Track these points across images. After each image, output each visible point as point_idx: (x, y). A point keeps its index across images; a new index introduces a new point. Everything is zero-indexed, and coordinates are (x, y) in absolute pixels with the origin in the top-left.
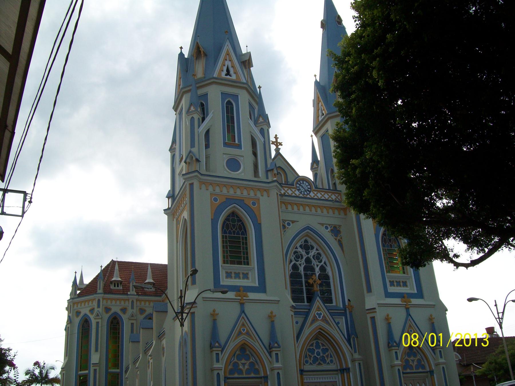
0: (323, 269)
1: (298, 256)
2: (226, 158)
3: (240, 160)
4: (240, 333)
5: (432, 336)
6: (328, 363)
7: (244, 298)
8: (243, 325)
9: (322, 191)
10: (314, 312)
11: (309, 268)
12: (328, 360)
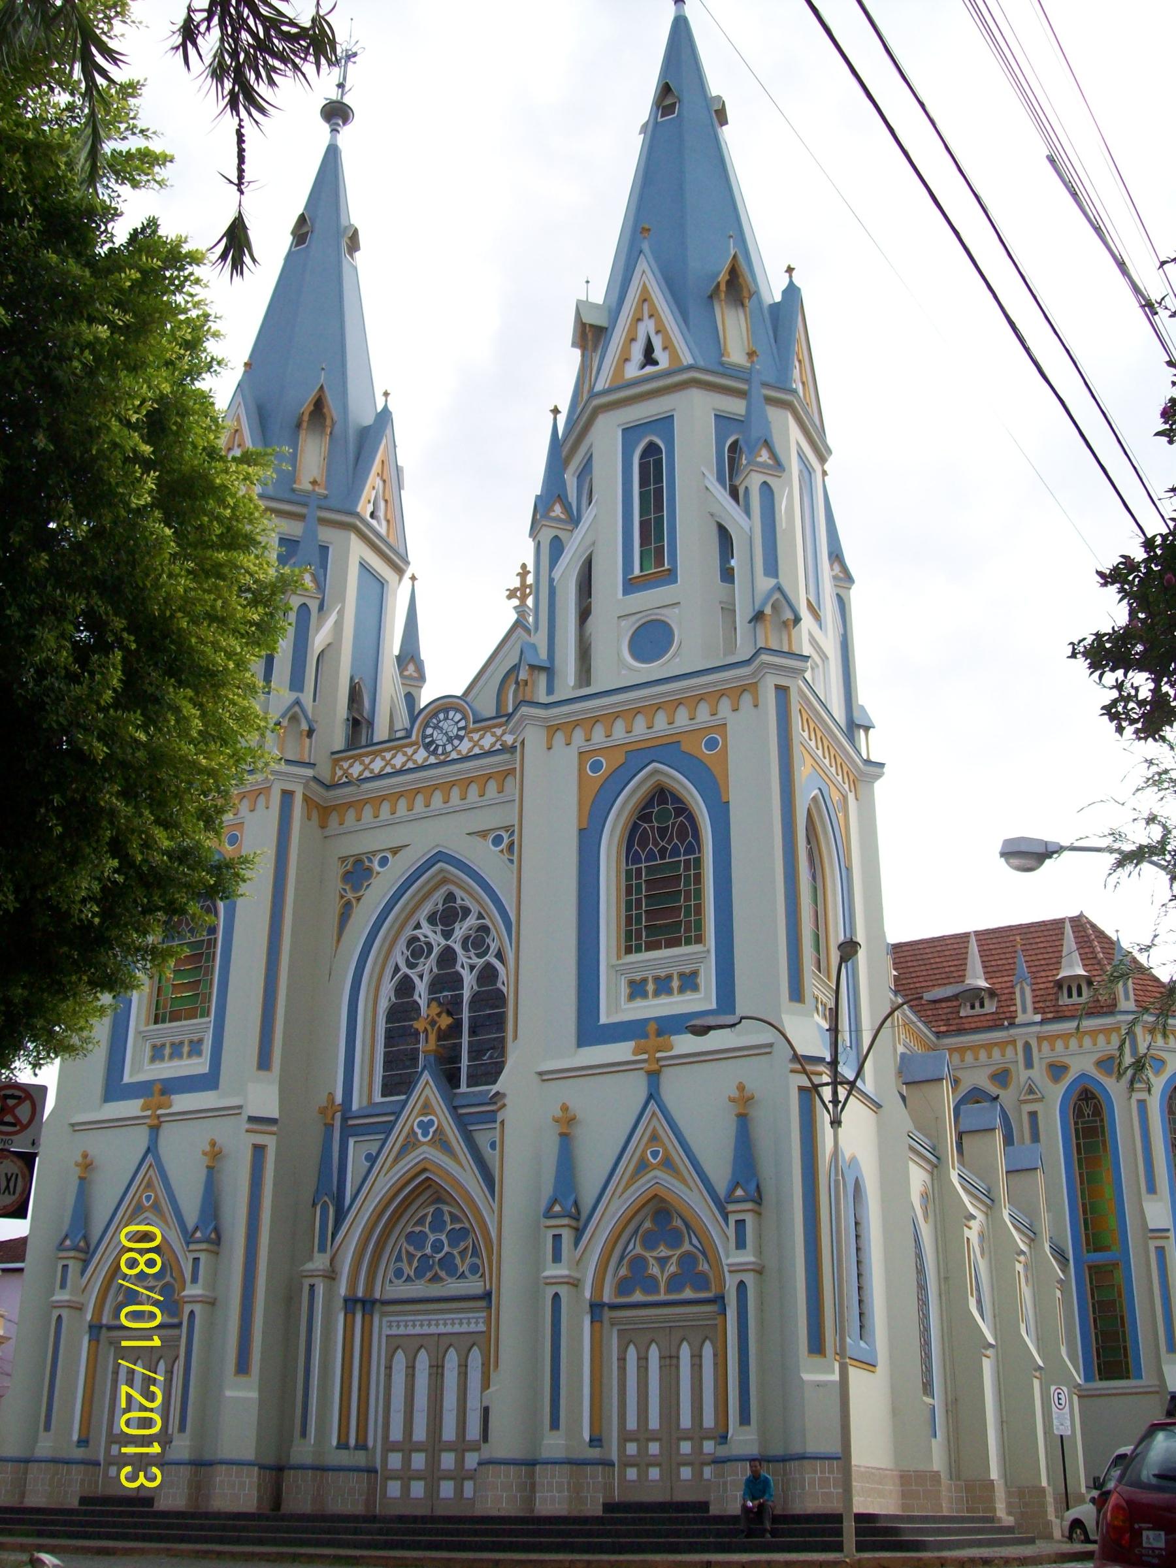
0: (488, 975)
1: (417, 949)
2: (628, 628)
3: (671, 617)
4: (642, 1166)
5: (153, 1316)
6: (462, 1276)
7: (658, 1055)
8: (654, 1138)
9: (495, 726)
10: (410, 1119)
11: (445, 981)
12: (463, 1268)
